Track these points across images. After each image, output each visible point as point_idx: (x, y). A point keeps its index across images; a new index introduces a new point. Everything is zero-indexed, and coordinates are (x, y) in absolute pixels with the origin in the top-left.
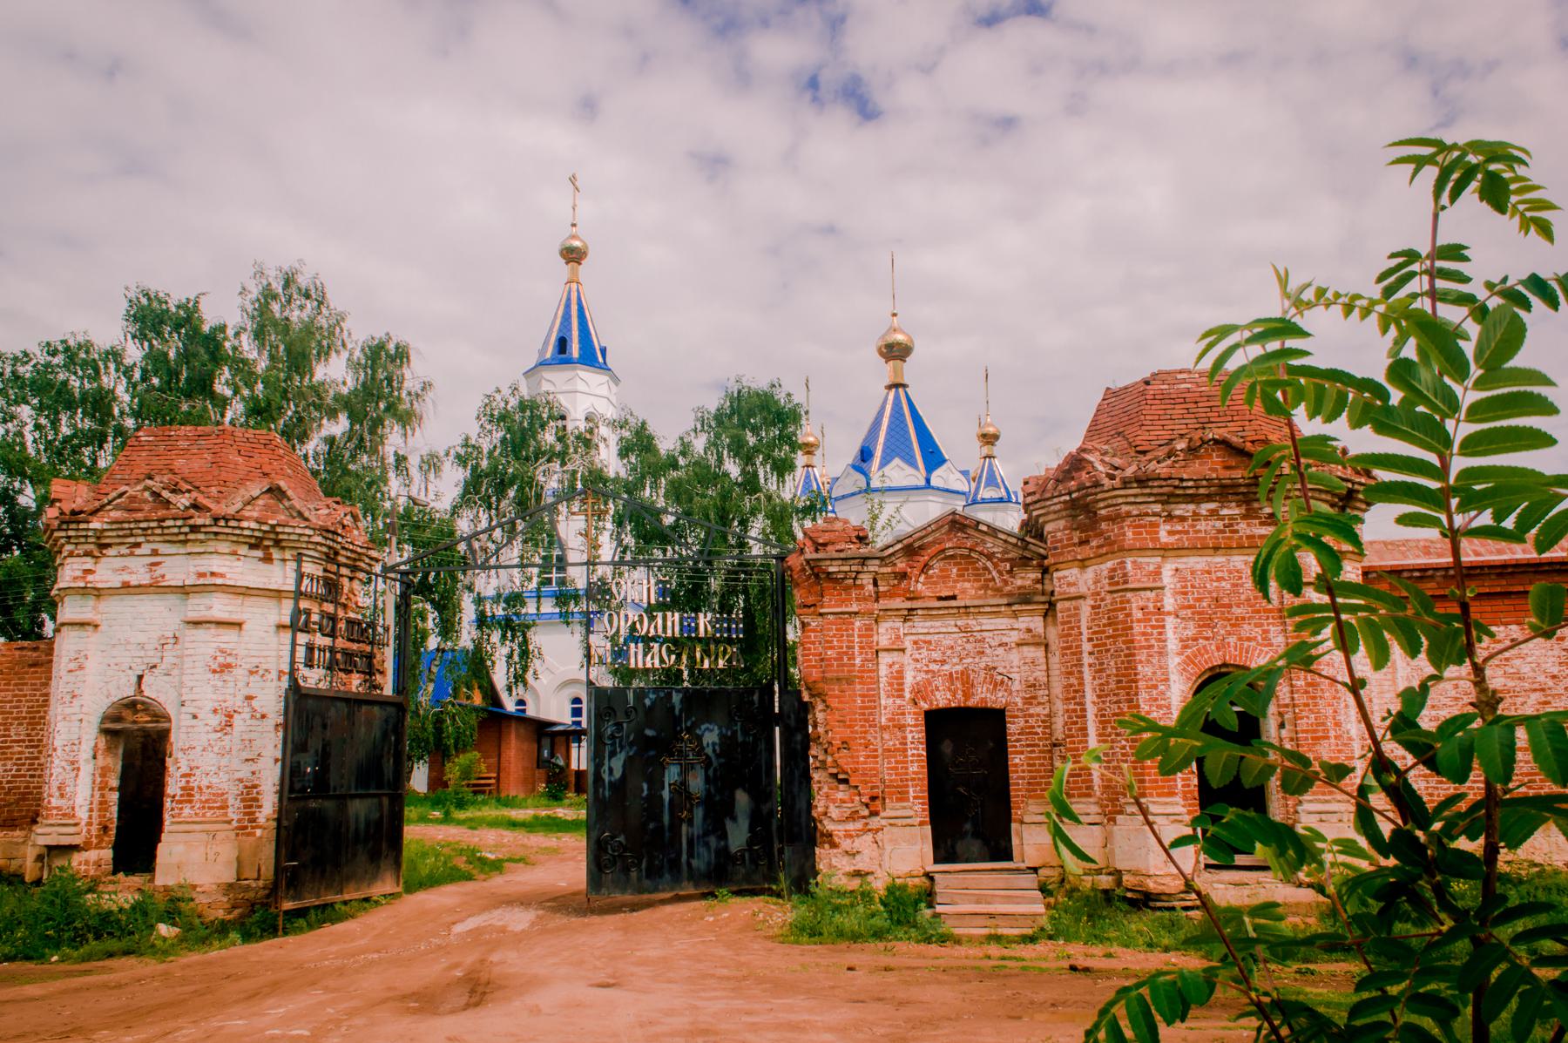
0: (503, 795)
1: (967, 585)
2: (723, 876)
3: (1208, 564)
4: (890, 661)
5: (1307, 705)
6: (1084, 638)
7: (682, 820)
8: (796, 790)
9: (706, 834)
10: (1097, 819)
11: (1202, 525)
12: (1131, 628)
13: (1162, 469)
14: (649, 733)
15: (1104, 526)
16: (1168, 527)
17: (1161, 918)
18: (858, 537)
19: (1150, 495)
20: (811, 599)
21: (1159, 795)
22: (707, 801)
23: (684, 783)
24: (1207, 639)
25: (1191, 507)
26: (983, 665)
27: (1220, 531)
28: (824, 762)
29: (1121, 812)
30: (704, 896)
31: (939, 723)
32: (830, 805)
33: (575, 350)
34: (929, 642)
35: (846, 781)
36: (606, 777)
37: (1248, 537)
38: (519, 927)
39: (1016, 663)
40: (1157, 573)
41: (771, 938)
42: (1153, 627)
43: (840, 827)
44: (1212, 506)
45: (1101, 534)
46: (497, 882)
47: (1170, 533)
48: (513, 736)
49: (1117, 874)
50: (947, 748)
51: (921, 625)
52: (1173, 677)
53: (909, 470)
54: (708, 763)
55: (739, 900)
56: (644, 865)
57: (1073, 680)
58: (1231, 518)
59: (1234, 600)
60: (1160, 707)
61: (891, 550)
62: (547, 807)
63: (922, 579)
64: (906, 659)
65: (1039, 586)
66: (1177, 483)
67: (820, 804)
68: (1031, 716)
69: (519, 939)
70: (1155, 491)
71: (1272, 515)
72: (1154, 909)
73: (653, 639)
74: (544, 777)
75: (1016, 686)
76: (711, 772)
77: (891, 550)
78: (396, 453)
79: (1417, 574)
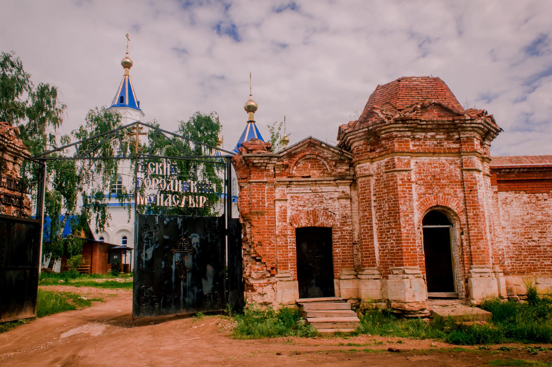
0: (93, 274)
1: (315, 172)
2: (202, 305)
3: (430, 160)
4: (280, 205)
5: (474, 224)
6: (372, 194)
7: (181, 279)
8: (235, 265)
9: (192, 286)
10: (378, 277)
11: (428, 143)
12: (397, 188)
13: (412, 115)
14: (166, 237)
15: (383, 142)
16: (413, 143)
17: (411, 322)
18: (267, 148)
19: (407, 127)
20: (245, 176)
21: (409, 265)
22: (193, 270)
23: (182, 262)
24: (430, 194)
25: (423, 134)
26: (322, 208)
27: (435, 146)
28: (249, 252)
29: (390, 274)
30: (191, 316)
31: (302, 234)
32: (252, 272)
33: (127, 102)
34: (298, 197)
35: (259, 261)
36: (144, 258)
37: (448, 149)
38: (96, 334)
39: (337, 207)
40: (408, 164)
41: (228, 336)
42: (407, 188)
43: (257, 282)
44: (433, 134)
45: (382, 146)
46: (88, 311)
47: (414, 146)
48: (98, 250)
49: (388, 302)
50: (304, 246)
51: (294, 189)
52: (415, 211)
54: (194, 252)
55: (208, 317)
56: (162, 301)
57: (366, 213)
58: (441, 139)
59: (442, 176)
60: (410, 225)
61: (282, 154)
62: (112, 278)
63: (295, 168)
64: (287, 204)
65: (348, 172)
66: (419, 122)
67: (247, 271)
68: (344, 230)
69: (96, 341)
70: (409, 125)
71: (459, 139)
72: (408, 318)
73: (170, 192)
74: (110, 266)
75: (337, 217)
76: (195, 256)
77: (282, 154)
78: (50, 134)
79: (508, 170)
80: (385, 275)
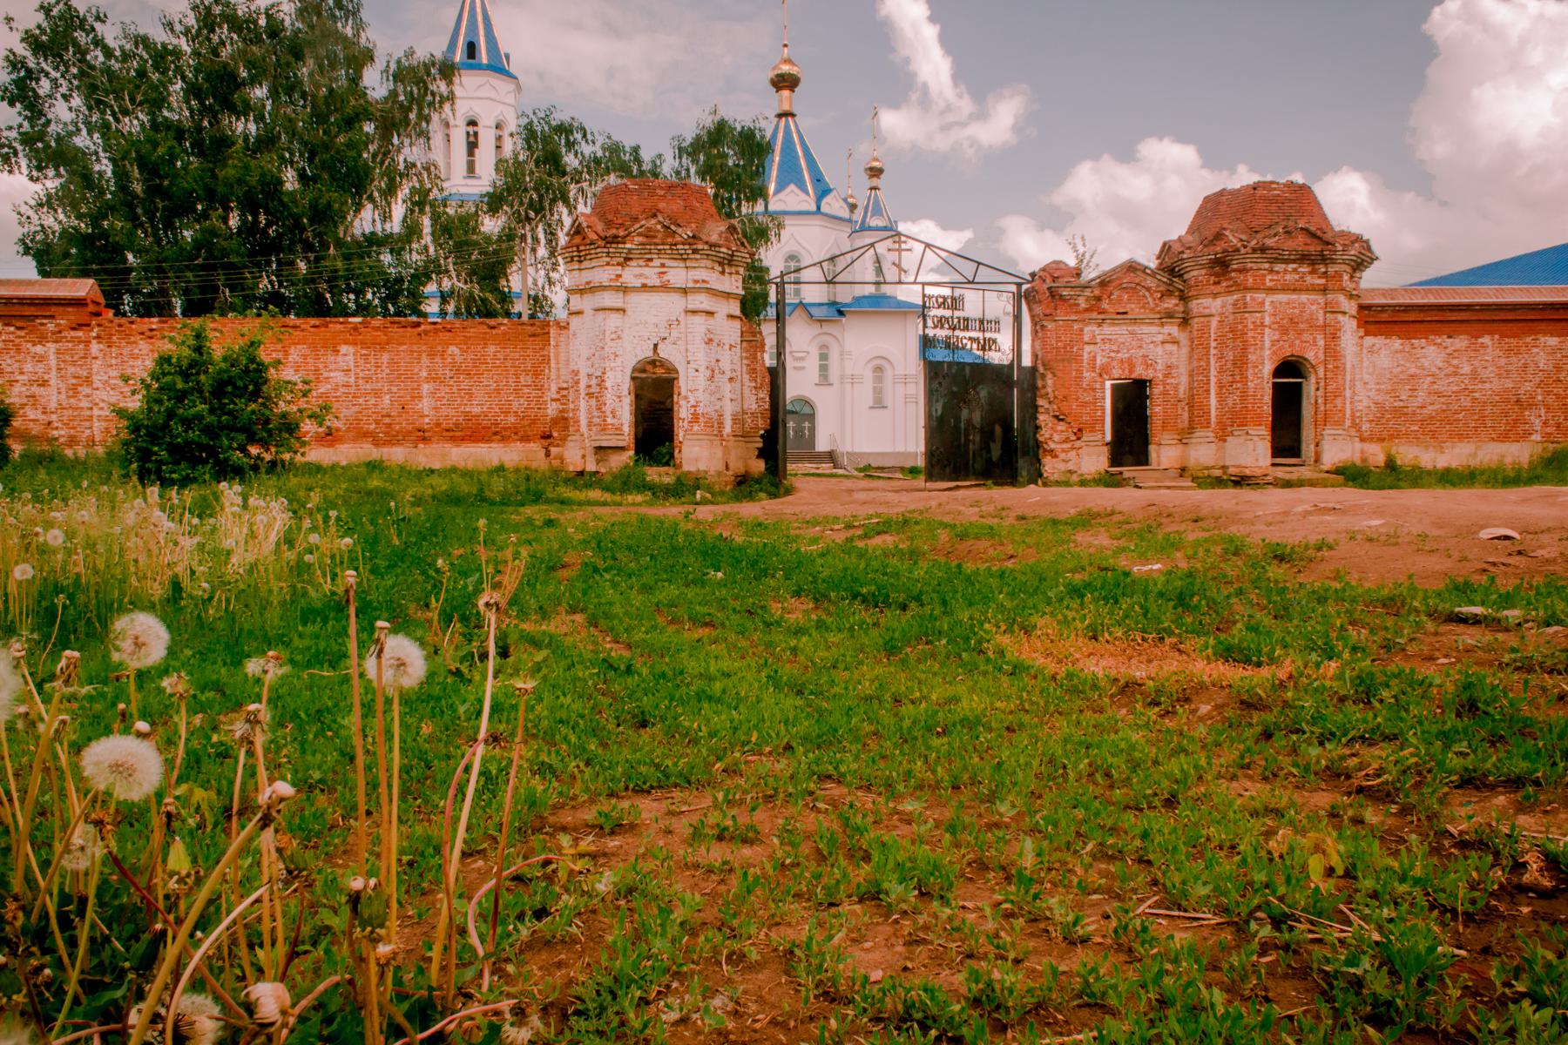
11: (1288, 277)
32: (1050, 432)
33: (483, 56)
40: (1262, 303)
51: (1107, 330)
53: (803, 196)
67: (1044, 435)
75: (1159, 367)
80: (1222, 438)
